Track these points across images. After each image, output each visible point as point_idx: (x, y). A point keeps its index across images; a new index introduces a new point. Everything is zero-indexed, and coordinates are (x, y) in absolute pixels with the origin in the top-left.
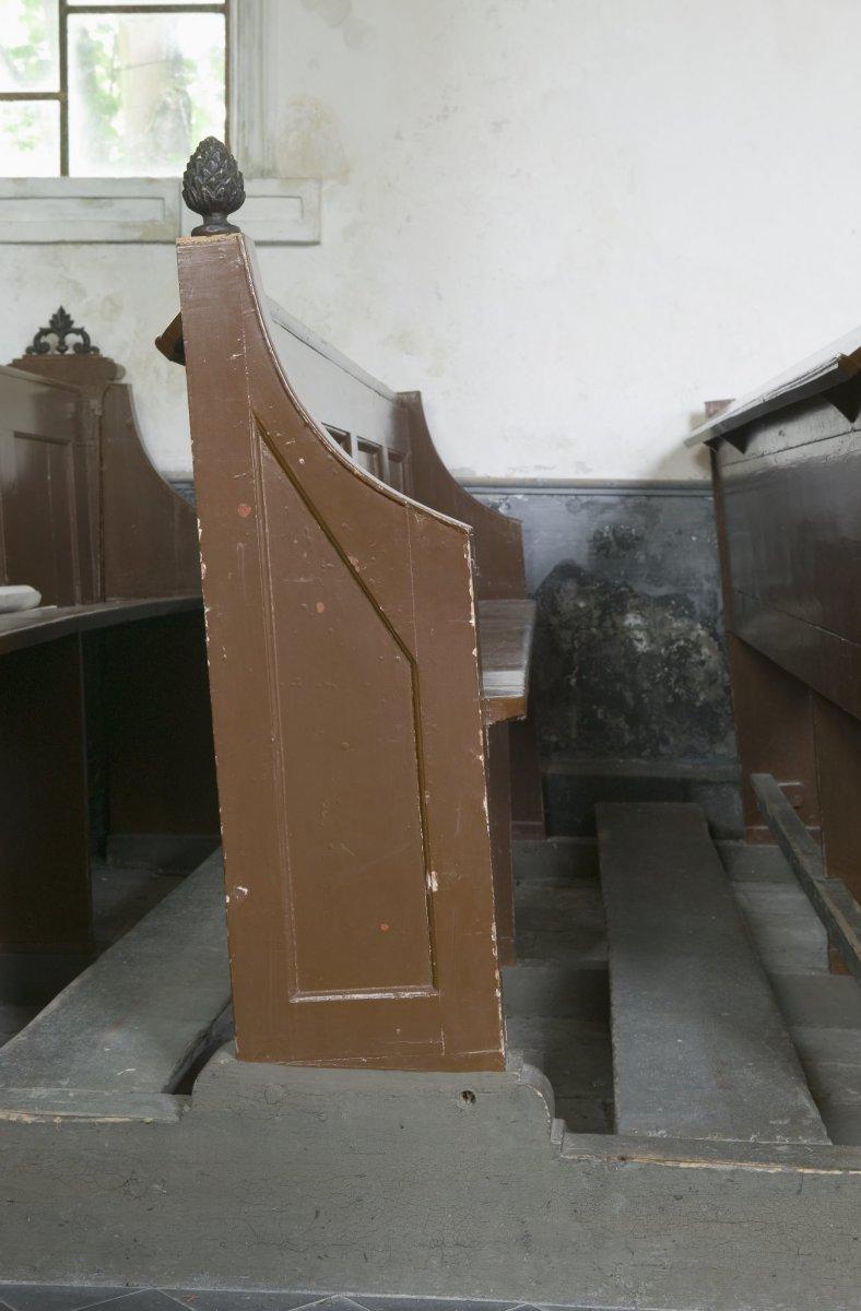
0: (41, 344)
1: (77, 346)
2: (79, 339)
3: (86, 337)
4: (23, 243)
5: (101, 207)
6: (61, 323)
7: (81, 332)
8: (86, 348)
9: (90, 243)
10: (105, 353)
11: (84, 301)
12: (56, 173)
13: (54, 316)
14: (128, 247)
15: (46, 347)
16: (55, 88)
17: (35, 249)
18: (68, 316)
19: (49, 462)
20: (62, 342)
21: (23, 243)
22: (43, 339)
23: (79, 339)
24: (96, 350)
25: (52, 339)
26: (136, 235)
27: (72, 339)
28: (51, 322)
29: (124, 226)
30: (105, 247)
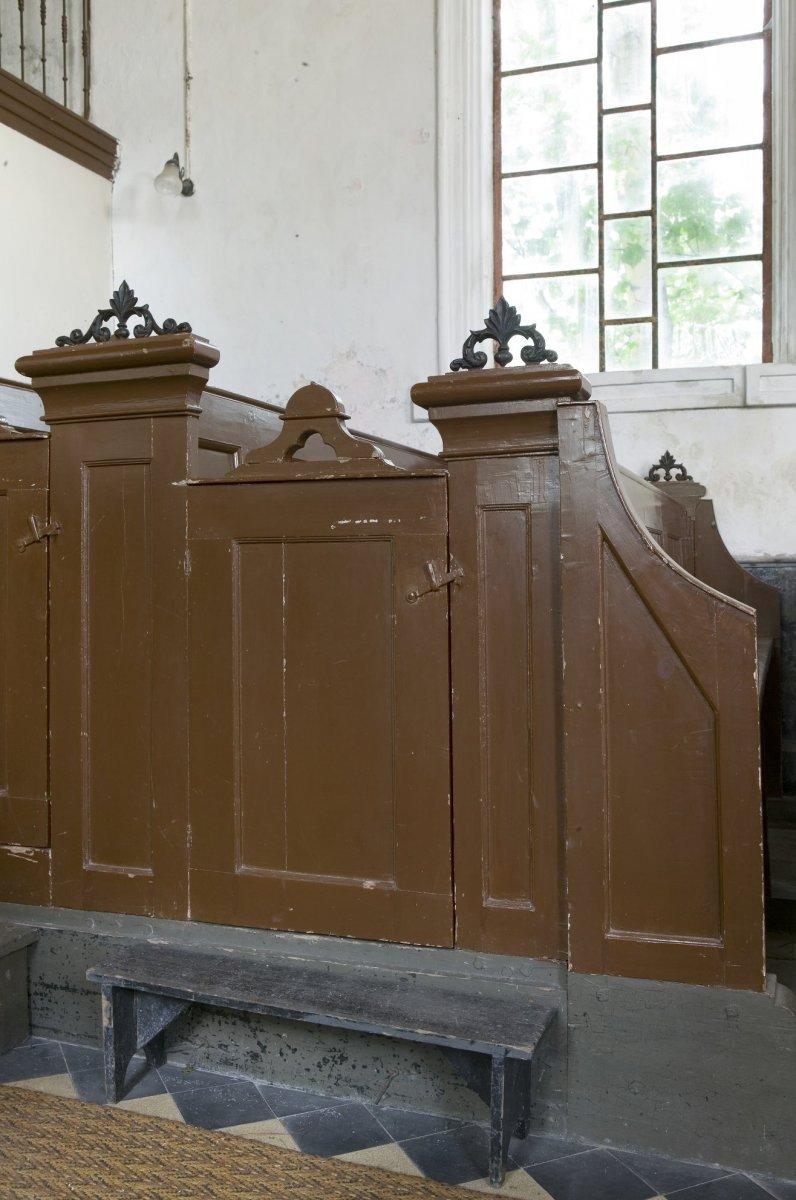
0: (474, 355)
1: (678, 476)
2: (680, 471)
3: (539, 340)
4: (639, 412)
5: (691, 386)
6: (667, 461)
7: (680, 467)
8: (684, 476)
9: (682, 410)
10: (695, 480)
11: (678, 447)
12: (649, 366)
13: (663, 457)
14: (707, 411)
15: (481, 359)
16: (649, 313)
17: (645, 415)
18: (512, 310)
19: (86, 509)
20: (668, 474)
21: (639, 412)
22: (655, 472)
23: (680, 471)
24: (690, 478)
25: (661, 472)
26: (714, 404)
27: (674, 472)
28: (489, 322)
29: (706, 398)
30: (692, 412)
